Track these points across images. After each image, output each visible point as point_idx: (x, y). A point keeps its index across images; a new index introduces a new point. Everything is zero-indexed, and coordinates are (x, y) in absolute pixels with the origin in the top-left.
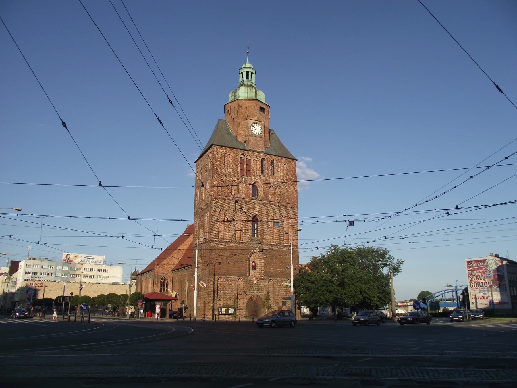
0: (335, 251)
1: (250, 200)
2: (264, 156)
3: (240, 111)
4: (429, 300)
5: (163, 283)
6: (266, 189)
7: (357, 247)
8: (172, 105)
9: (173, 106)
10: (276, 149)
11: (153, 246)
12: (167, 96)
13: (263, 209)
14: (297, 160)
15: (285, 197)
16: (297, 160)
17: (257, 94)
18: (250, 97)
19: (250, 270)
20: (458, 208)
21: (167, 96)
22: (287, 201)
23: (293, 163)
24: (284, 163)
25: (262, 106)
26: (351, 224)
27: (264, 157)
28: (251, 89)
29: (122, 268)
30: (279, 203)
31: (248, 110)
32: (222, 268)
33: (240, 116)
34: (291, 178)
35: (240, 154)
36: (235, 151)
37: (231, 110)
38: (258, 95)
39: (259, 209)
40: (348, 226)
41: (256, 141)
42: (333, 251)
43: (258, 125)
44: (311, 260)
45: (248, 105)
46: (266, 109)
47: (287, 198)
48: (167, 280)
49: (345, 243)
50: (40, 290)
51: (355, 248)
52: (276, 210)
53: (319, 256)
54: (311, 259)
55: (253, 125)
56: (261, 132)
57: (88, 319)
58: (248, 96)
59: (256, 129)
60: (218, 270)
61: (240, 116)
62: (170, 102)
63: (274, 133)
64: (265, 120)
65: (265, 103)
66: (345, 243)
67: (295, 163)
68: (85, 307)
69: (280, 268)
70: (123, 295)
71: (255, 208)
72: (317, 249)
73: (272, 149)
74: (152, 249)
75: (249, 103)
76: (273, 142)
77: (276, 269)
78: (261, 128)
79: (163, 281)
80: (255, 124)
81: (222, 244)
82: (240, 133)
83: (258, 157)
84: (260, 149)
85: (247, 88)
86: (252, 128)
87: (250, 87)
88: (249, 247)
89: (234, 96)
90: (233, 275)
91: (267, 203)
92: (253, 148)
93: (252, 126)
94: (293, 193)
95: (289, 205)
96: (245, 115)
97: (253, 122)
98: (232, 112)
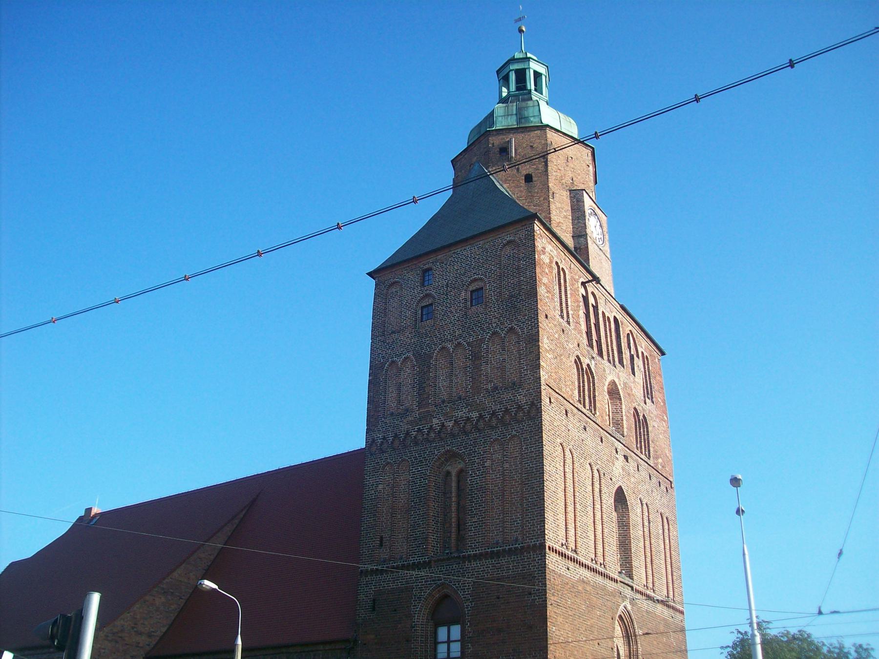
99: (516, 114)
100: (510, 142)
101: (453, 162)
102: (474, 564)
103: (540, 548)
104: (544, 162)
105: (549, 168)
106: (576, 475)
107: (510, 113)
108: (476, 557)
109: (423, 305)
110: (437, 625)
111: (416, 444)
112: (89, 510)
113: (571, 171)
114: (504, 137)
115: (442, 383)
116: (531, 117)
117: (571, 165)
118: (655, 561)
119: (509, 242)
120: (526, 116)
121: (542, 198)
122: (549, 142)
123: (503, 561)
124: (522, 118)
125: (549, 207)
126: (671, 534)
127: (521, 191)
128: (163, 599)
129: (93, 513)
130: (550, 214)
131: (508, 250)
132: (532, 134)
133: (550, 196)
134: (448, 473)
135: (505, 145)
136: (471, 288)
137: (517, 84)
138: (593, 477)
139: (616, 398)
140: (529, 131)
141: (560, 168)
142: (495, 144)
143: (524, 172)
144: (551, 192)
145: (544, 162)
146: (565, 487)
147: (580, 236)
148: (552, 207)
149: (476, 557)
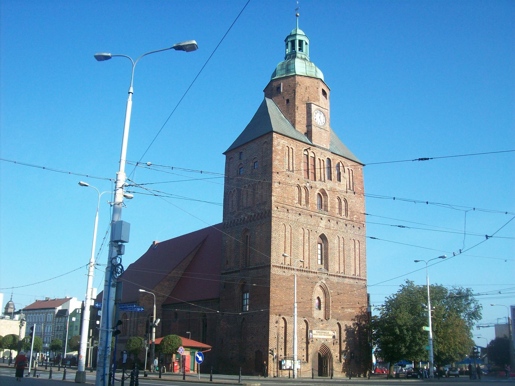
0: (408, 288)
1: (315, 213)
2: (331, 157)
3: (298, 91)
6: (332, 200)
22: (355, 219)
23: (360, 169)
31: (309, 91)
33: (299, 97)
34: (358, 188)
36: (298, 144)
41: (320, 134)
45: (308, 85)
47: (354, 215)
50: (346, 325)
57: (122, 374)
58: (307, 72)
61: (299, 97)
68: (201, 356)
70: (5, 336)
75: (309, 82)
82: (299, 120)
83: (323, 156)
84: (325, 145)
85: (304, 62)
88: (314, 278)
92: (317, 143)
94: (361, 209)
95: (357, 223)
96: (304, 97)
99: (285, 68)
100: (280, 84)
101: (264, 91)
102: (252, 271)
103: (268, 266)
104: (294, 93)
105: (296, 95)
106: (292, 235)
107: (283, 68)
108: (252, 269)
109: (240, 167)
110: (243, 293)
111: (237, 225)
112: (154, 242)
113: (308, 93)
114: (278, 82)
115: (245, 201)
116: (291, 69)
117: (308, 90)
118: (347, 261)
119: (266, 142)
120: (289, 69)
121: (292, 111)
122: (297, 82)
123: (260, 270)
124: (288, 70)
125: (295, 114)
126: (360, 247)
127: (284, 108)
128: (168, 283)
129: (155, 244)
130: (295, 117)
131: (265, 145)
132: (290, 79)
133: (296, 109)
134: (247, 236)
135: (279, 86)
136: (254, 161)
137: (292, 47)
138: (304, 233)
139: (325, 195)
140: (288, 78)
141: (302, 94)
142: (275, 86)
143: (286, 98)
144: (296, 107)
145: (294, 93)
146: (285, 241)
147: (309, 126)
148: (297, 114)
149: (252, 269)
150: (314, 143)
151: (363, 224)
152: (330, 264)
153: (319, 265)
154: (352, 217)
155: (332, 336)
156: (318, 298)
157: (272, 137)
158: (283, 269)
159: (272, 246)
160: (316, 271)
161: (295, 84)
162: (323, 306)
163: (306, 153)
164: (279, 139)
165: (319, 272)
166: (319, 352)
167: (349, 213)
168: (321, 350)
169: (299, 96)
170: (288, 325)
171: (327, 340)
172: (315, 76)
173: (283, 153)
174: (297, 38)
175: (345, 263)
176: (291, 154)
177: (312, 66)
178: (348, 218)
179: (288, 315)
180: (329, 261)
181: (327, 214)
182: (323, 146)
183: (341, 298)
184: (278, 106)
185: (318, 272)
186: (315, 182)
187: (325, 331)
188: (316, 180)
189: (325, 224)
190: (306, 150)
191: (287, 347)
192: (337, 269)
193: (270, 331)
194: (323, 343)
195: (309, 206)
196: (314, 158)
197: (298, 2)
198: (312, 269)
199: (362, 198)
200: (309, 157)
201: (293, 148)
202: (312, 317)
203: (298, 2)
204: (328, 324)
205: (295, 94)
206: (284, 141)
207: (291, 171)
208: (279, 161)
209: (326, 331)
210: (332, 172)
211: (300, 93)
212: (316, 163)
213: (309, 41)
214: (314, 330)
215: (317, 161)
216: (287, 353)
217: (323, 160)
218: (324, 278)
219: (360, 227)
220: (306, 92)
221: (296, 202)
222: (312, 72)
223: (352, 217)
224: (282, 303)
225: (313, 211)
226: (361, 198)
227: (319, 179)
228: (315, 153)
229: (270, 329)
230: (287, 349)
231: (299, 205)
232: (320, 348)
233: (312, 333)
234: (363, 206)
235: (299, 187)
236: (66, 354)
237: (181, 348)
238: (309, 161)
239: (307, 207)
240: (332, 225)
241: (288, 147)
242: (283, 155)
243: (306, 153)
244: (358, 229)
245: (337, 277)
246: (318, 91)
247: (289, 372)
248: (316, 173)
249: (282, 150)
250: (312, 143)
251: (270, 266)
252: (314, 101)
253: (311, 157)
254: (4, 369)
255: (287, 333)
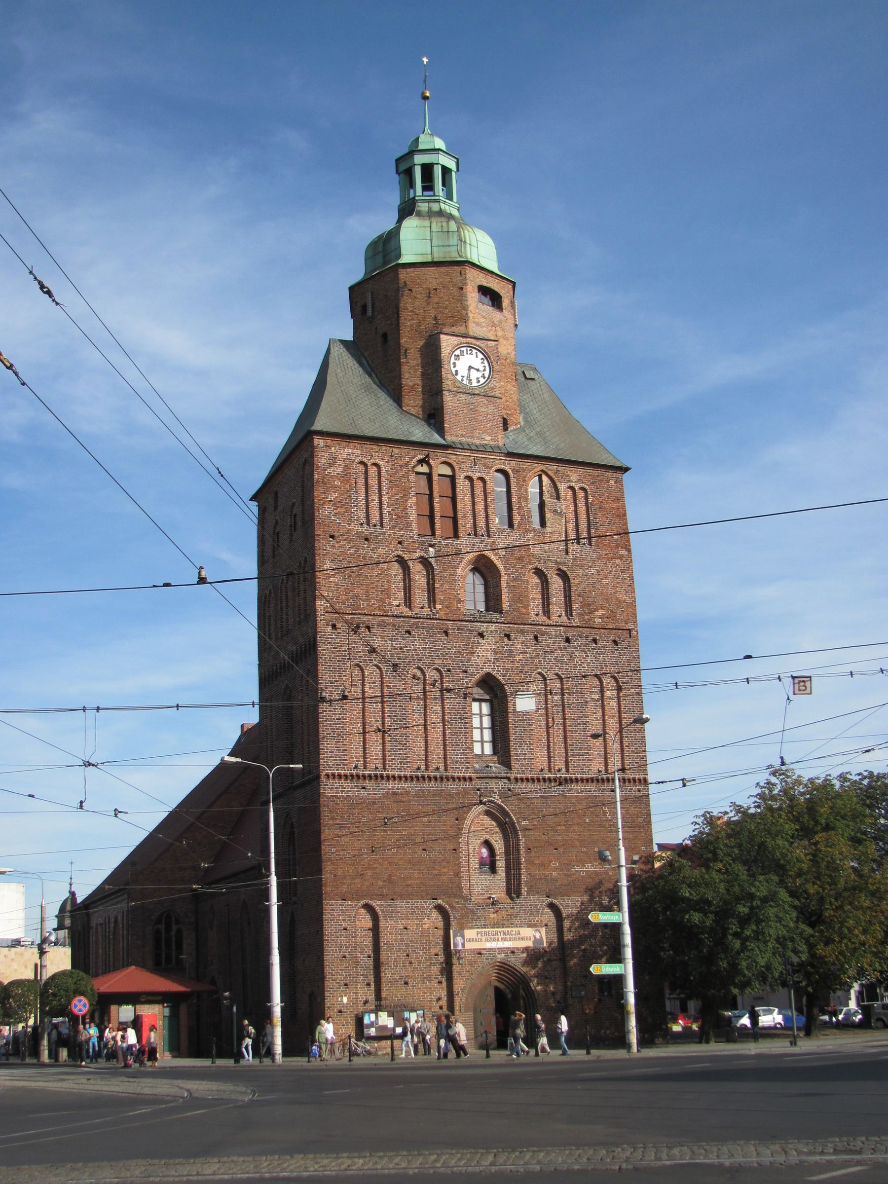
4: (286, 882)
5: (163, 934)
6: (515, 580)
7: (866, 774)
8: (54, 300)
9: (57, 304)
10: (548, 433)
11: (81, 802)
12: (31, 273)
13: (511, 653)
14: (625, 470)
15: (590, 605)
16: (625, 470)
17: (465, 242)
18: (442, 255)
19: (472, 873)
20: (208, 580)
21: (31, 273)
23: (612, 482)
24: (579, 480)
25: (484, 284)
26: (804, 688)
27: (504, 464)
28: (444, 224)
29: (23, 890)
30: (569, 629)
32: (369, 873)
35: (415, 460)
37: (373, 305)
38: (468, 246)
39: (495, 652)
40: (792, 697)
42: (774, 792)
43: (474, 351)
44: (697, 826)
45: (434, 285)
46: (502, 293)
47: (596, 610)
48: (177, 922)
49: (782, 758)
51: (857, 778)
52: (558, 654)
53: (726, 813)
54: (696, 823)
55: (457, 352)
56: (487, 374)
59: (470, 368)
60: (354, 879)
62: (45, 293)
63: (536, 377)
64: (500, 333)
65: (496, 271)
66: (782, 758)
67: (619, 482)
69: (582, 863)
71: (479, 651)
72: (684, 785)
73: (532, 434)
74: (81, 813)
76: (535, 411)
77: (570, 864)
78: (486, 364)
79: (162, 927)
80: (464, 349)
81: (364, 788)
82: (411, 384)
83: (482, 468)
84: (489, 438)
85: (427, 223)
86: (452, 366)
87: (439, 219)
89: (381, 254)
90: (411, 897)
91: (522, 632)
92: (463, 436)
93: (453, 356)
97: (456, 343)
98: (376, 313)
105: (402, 320)
117: (435, 300)
144: (403, 351)
148: (405, 369)
150: (450, 438)
151: (630, 630)
152: (516, 750)
153: (489, 755)
154: (586, 617)
155: (533, 939)
156: (487, 844)
157: (313, 447)
158: (361, 781)
159: (321, 726)
160: (467, 775)
161: (398, 290)
162: (501, 864)
163: (424, 469)
164: (333, 448)
165: (478, 775)
166: (497, 984)
167: (576, 607)
168: (504, 975)
169: (410, 320)
170: (382, 923)
171: (516, 951)
172: (458, 256)
173: (348, 481)
174: (416, 162)
175: (569, 743)
176: (373, 482)
177: (448, 232)
178: (576, 621)
179: (382, 897)
180: (512, 743)
181: (501, 621)
182: (484, 439)
183: (560, 838)
184: (366, 354)
185: (473, 775)
186: (456, 542)
187: (506, 929)
188: (461, 535)
189: (494, 647)
190: (421, 462)
191: (384, 979)
192: (541, 761)
193: (325, 943)
194: (504, 961)
195: (438, 606)
196: (453, 478)
197: (425, 60)
198: (454, 771)
199: (621, 560)
200: (435, 478)
201: (381, 463)
202: (462, 897)
203: (425, 60)
204: (516, 910)
205: (398, 317)
206: (351, 451)
207: (375, 525)
208: (336, 504)
209: (509, 929)
210: (514, 504)
211: (412, 311)
212: (458, 490)
213: (456, 161)
214: (470, 928)
215: (462, 485)
216: (384, 995)
217: (482, 479)
218: (496, 790)
219: (617, 639)
220: (428, 304)
221: (396, 603)
222: (449, 246)
223: (586, 617)
224: (360, 869)
225: (452, 619)
226: (618, 561)
227: (470, 530)
228: (454, 464)
229: (326, 938)
230: (383, 985)
231: (405, 611)
232: (495, 975)
233: (463, 938)
234: (626, 581)
235: (401, 561)
236: (867, 1002)
237: (80, 1001)
238: (436, 487)
239: (431, 611)
240: (519, 646)
241: (362, 463)
242: (347, 486)
243: (424, 469)
244: (610, 645)
245: (542, 783)
246: (462, 295)
247: (392, 1043)
248: (460, 516)
249: (345, 476)
250: (444, 439)
251: (318, 777)
252: (453, 326)
253: (439, 475)
254: (294, 1066)
255: (382, 944)
